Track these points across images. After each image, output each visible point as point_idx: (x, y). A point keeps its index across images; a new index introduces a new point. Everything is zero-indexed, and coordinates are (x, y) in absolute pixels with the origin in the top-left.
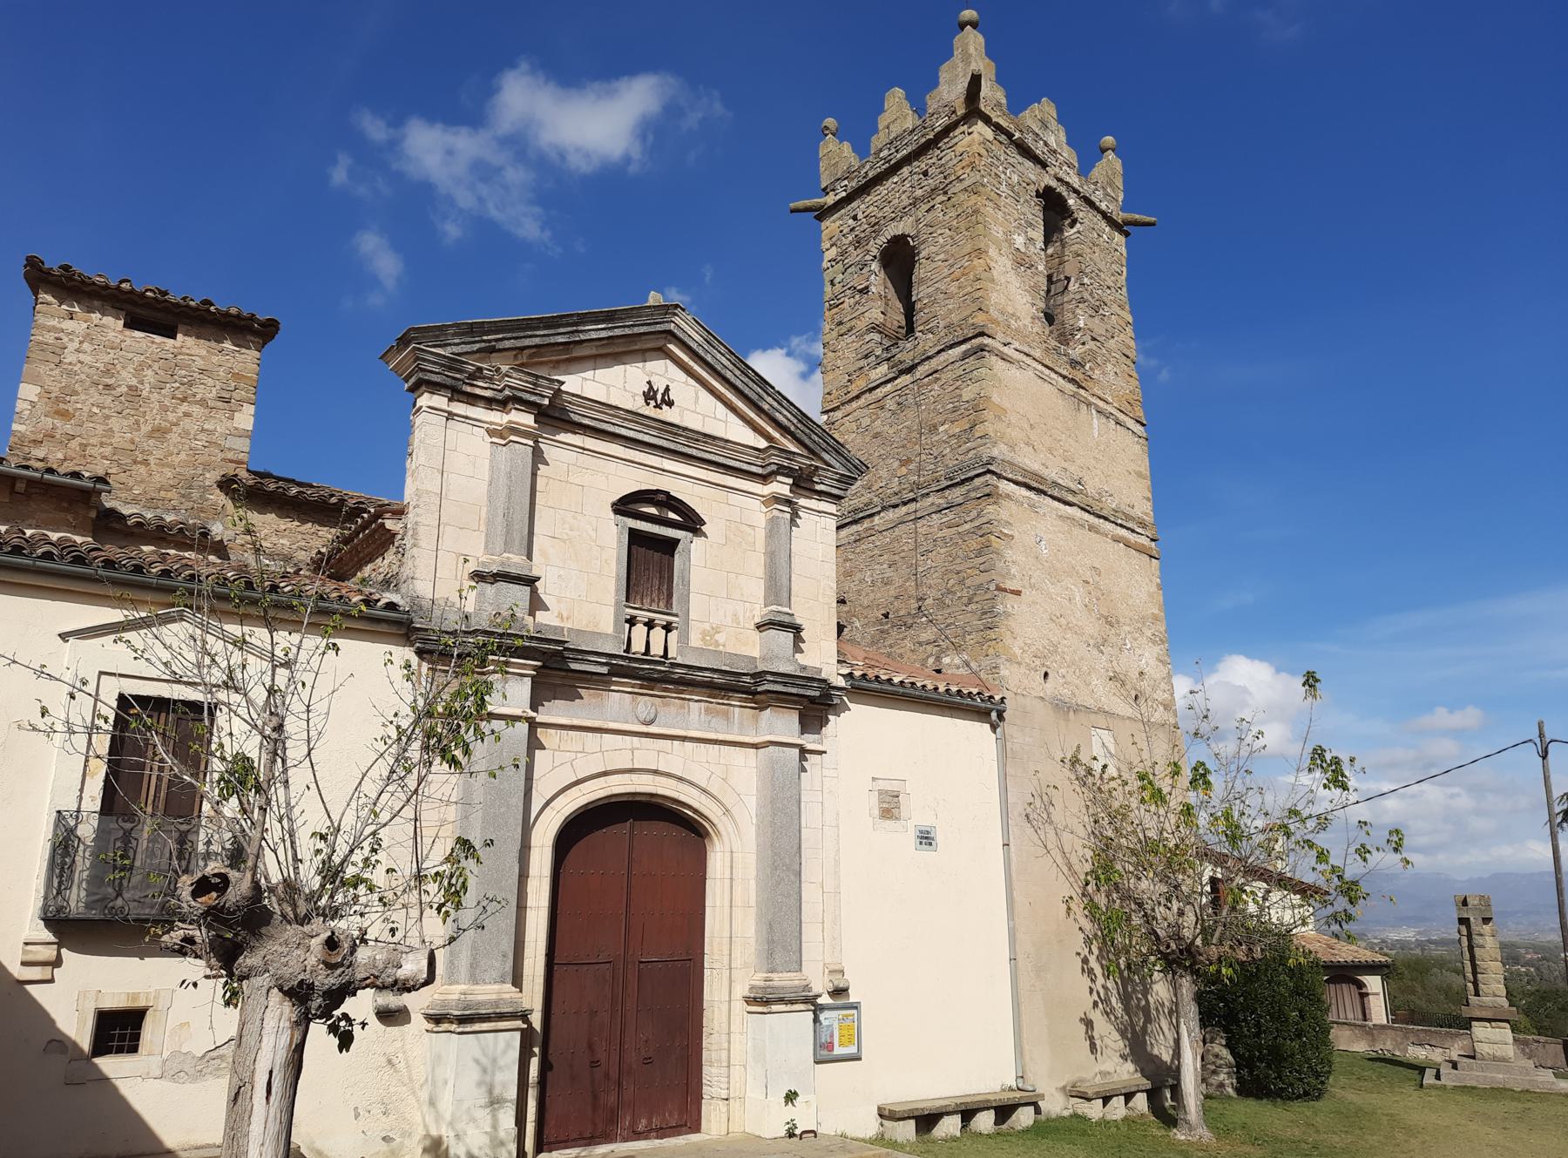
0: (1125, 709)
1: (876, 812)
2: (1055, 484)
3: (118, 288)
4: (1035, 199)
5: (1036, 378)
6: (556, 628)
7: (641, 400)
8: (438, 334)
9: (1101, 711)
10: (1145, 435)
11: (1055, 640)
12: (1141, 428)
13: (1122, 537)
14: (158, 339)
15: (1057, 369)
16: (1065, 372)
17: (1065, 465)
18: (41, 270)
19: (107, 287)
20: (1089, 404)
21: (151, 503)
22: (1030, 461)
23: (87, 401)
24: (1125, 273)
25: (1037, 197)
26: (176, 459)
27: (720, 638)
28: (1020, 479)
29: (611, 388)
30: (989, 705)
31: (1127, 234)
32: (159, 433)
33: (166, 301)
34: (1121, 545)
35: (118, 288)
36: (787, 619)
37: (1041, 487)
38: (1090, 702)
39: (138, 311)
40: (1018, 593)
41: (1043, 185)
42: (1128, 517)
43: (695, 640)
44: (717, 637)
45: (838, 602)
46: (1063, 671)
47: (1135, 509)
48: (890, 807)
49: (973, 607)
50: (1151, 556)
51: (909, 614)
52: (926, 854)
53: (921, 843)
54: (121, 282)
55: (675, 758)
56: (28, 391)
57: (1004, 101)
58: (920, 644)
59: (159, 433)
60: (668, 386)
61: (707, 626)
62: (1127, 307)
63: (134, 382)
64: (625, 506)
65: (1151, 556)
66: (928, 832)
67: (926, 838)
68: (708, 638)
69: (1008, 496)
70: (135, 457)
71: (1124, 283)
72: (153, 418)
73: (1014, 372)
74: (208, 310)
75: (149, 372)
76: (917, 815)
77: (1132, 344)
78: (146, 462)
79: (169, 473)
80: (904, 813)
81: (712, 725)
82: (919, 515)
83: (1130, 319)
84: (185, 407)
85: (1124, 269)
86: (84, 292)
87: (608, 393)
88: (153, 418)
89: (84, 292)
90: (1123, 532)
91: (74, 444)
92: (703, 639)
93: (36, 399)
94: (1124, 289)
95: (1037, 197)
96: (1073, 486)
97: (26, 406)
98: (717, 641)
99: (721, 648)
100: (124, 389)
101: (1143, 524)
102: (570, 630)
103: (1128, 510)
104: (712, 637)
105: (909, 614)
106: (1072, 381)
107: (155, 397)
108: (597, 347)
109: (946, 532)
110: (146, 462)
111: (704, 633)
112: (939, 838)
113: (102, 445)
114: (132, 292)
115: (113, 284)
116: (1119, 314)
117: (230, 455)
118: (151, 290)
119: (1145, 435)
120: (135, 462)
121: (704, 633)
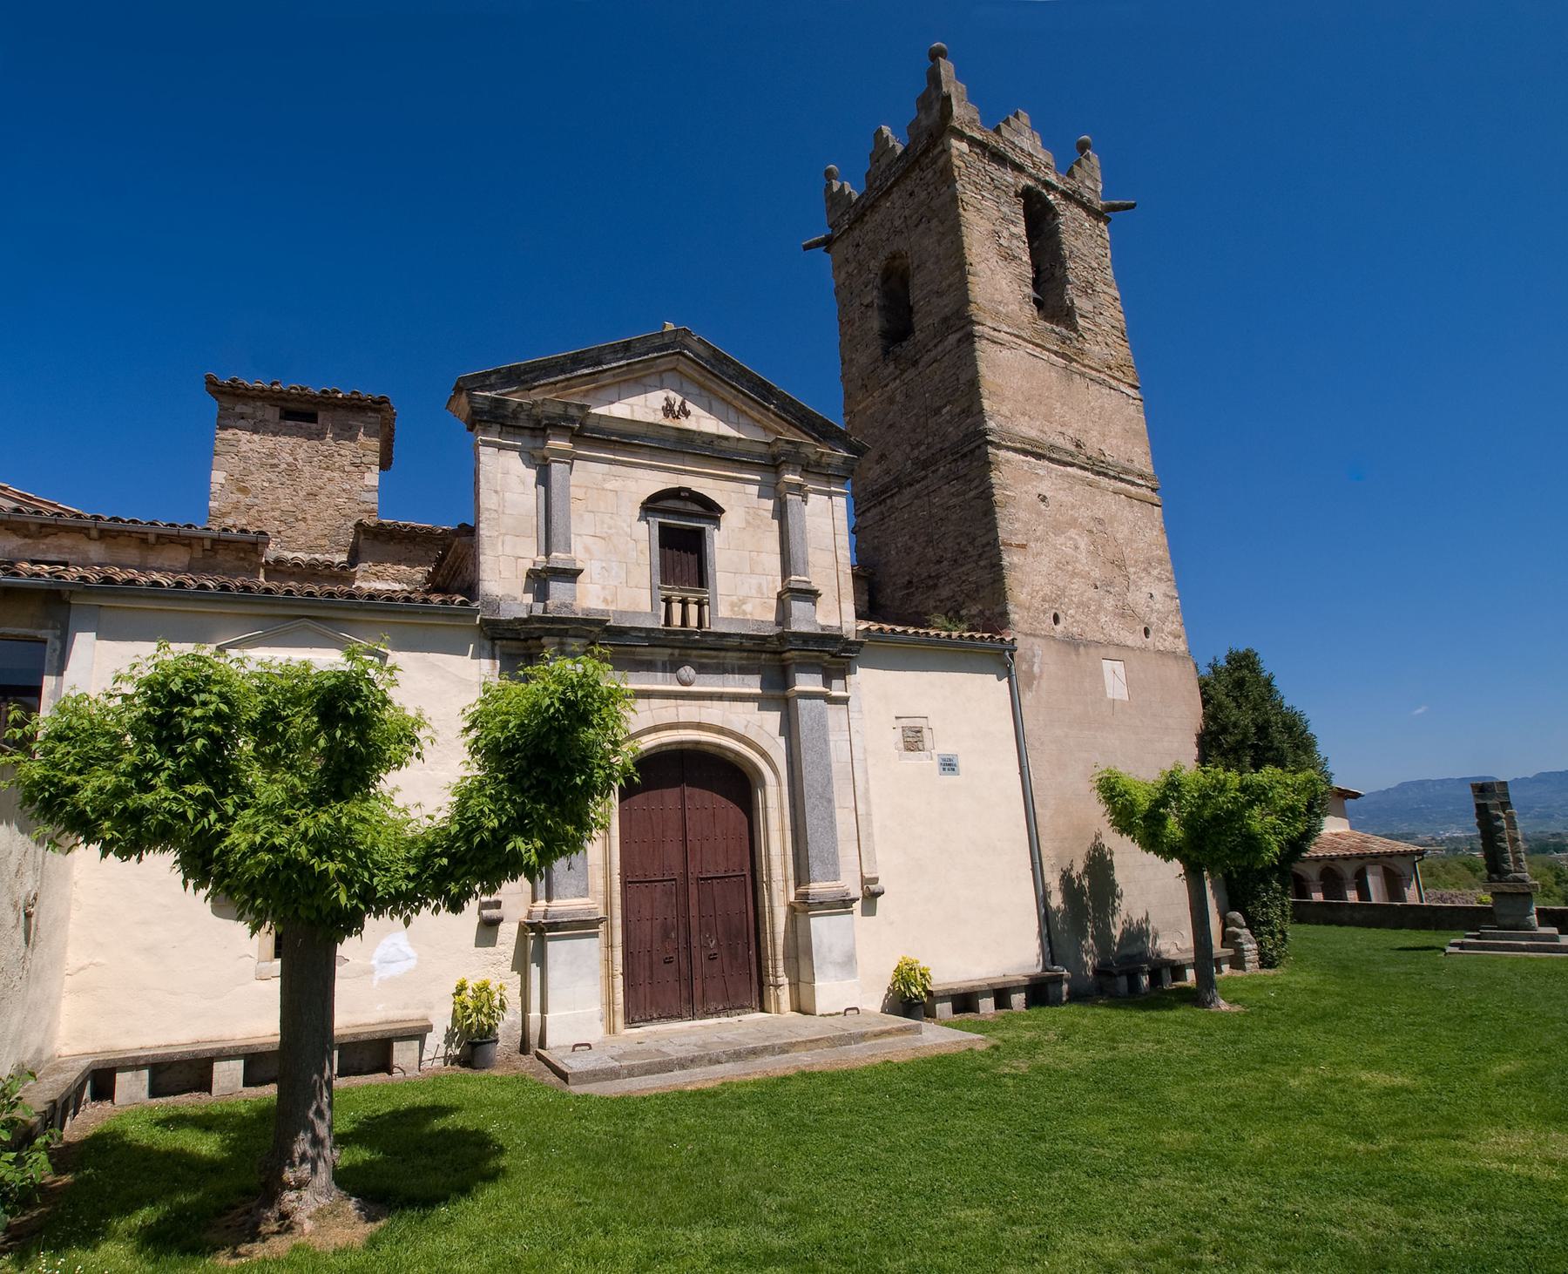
0: (1134, 639)
1: (901, 745)
2: (1053, 448)
3: (289, 391)
4: (1015, 199)
5: (1027, 356)
6: (603, 611)
7: (661, 414)
8: (482, 381)
9: (1111, 644)
10: (1139, 396)
11: (1061, 584)
12: (1136, 391)
13: (1121, 489)
14: (304, 424)
15: (1048, 346)
16: (1055, 348)
17: (1063, 430)
18: (216, 385)
19: (263, 390)
20: (1082, 375)
21: (310, 549)
22: (1027, 429)
23: (258, 480)
24: (1109, 255)
25: (1016, 196)
26: (325, 515)
27: (748, 608)
28: (1019, 445)
29: (635, 407)
30: (1003, 647)
31: (1107, 221)
32: (312, 495)
33: (306, 395)
34: (1123, 496)
35: (289, 391)
36: (804, 586)
37: (1040, 451)
38: (1099, 637)
39: (289, 405)
40: (1023, 546)
41: (1021, 186)
42: (1127, 471)
43: (723, 611)
44: (744, 607)
45: (1483, 789)
46: (1071, 612)
47: (1136, 463)
48: (913, 740)
49: (982, 563)
50: (1153, 504)
51: (930, 577)
52: (949, 779)
53: (944, 769)
54: (273, 384)
55: (713, 713)
56: (218, 477)
57: (977, 117)
58: (941, 601)
59: (312, 495)
60: (1147, 637)
61: (734, 598)
62: (1114, 285)
63: (290, 459)
64: (652, 506)
65: (1153, 504)
66: (950, 760)
67: (949, 765)
68: (736, 609)
69: (1008, 461)
70: (292, 518)
71: (1109, 264)
72: (306, 486)
73: (1006, 353)
74: (336, 398)
75: (301, 451)
76: (942, 745)
77: (1121, 316)
78: (304, 519)
79: (320, 525)
80: (928, 744)
81: (746, 681)
82: (931, 489)
83: (1117, 295)
84: (328, 474)
85: (1108, 251)
86: (249, 397)
87: (632, 411)
88: (306, 486)
89: (249, 397)
90: (1122, 485)
91: (253, 512)
92: (732, 610)
93: (224, 482)
94: (1110, 271)
95: (1016, 196)
96: (1073, 448)
97: (219, 487)
98: (744, 611)
99: (749, 617)
100: (283, 466)
101: (1141, 476)
102: (614, 612)
103: (1127, 464)
104: (740, 607)
105: (930, 577)
106: (1063, 356)
107: (307, 468)
108: (614, 375)
109: (954, 501)
110: (304, 519)
111: (733, 605)
112: (962, 764)
113: (273, 510)
114: (281, 391)
115: (267, 386)
116: (1109, 292)
117: (364, 507)
118: (294, 388)
119: (1139, 396)
120: (297, 520)
121: (733, 605)
